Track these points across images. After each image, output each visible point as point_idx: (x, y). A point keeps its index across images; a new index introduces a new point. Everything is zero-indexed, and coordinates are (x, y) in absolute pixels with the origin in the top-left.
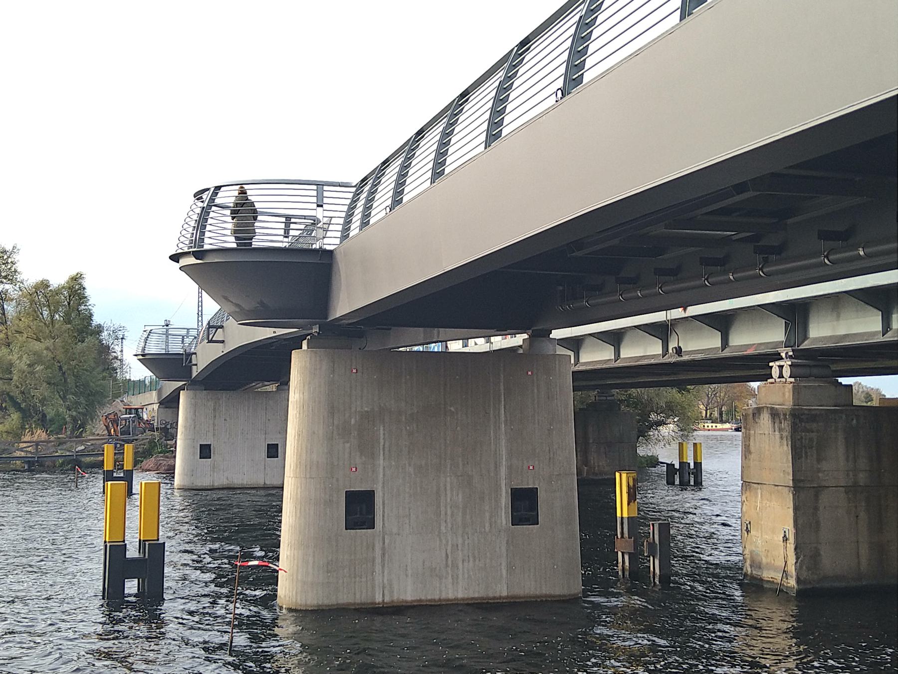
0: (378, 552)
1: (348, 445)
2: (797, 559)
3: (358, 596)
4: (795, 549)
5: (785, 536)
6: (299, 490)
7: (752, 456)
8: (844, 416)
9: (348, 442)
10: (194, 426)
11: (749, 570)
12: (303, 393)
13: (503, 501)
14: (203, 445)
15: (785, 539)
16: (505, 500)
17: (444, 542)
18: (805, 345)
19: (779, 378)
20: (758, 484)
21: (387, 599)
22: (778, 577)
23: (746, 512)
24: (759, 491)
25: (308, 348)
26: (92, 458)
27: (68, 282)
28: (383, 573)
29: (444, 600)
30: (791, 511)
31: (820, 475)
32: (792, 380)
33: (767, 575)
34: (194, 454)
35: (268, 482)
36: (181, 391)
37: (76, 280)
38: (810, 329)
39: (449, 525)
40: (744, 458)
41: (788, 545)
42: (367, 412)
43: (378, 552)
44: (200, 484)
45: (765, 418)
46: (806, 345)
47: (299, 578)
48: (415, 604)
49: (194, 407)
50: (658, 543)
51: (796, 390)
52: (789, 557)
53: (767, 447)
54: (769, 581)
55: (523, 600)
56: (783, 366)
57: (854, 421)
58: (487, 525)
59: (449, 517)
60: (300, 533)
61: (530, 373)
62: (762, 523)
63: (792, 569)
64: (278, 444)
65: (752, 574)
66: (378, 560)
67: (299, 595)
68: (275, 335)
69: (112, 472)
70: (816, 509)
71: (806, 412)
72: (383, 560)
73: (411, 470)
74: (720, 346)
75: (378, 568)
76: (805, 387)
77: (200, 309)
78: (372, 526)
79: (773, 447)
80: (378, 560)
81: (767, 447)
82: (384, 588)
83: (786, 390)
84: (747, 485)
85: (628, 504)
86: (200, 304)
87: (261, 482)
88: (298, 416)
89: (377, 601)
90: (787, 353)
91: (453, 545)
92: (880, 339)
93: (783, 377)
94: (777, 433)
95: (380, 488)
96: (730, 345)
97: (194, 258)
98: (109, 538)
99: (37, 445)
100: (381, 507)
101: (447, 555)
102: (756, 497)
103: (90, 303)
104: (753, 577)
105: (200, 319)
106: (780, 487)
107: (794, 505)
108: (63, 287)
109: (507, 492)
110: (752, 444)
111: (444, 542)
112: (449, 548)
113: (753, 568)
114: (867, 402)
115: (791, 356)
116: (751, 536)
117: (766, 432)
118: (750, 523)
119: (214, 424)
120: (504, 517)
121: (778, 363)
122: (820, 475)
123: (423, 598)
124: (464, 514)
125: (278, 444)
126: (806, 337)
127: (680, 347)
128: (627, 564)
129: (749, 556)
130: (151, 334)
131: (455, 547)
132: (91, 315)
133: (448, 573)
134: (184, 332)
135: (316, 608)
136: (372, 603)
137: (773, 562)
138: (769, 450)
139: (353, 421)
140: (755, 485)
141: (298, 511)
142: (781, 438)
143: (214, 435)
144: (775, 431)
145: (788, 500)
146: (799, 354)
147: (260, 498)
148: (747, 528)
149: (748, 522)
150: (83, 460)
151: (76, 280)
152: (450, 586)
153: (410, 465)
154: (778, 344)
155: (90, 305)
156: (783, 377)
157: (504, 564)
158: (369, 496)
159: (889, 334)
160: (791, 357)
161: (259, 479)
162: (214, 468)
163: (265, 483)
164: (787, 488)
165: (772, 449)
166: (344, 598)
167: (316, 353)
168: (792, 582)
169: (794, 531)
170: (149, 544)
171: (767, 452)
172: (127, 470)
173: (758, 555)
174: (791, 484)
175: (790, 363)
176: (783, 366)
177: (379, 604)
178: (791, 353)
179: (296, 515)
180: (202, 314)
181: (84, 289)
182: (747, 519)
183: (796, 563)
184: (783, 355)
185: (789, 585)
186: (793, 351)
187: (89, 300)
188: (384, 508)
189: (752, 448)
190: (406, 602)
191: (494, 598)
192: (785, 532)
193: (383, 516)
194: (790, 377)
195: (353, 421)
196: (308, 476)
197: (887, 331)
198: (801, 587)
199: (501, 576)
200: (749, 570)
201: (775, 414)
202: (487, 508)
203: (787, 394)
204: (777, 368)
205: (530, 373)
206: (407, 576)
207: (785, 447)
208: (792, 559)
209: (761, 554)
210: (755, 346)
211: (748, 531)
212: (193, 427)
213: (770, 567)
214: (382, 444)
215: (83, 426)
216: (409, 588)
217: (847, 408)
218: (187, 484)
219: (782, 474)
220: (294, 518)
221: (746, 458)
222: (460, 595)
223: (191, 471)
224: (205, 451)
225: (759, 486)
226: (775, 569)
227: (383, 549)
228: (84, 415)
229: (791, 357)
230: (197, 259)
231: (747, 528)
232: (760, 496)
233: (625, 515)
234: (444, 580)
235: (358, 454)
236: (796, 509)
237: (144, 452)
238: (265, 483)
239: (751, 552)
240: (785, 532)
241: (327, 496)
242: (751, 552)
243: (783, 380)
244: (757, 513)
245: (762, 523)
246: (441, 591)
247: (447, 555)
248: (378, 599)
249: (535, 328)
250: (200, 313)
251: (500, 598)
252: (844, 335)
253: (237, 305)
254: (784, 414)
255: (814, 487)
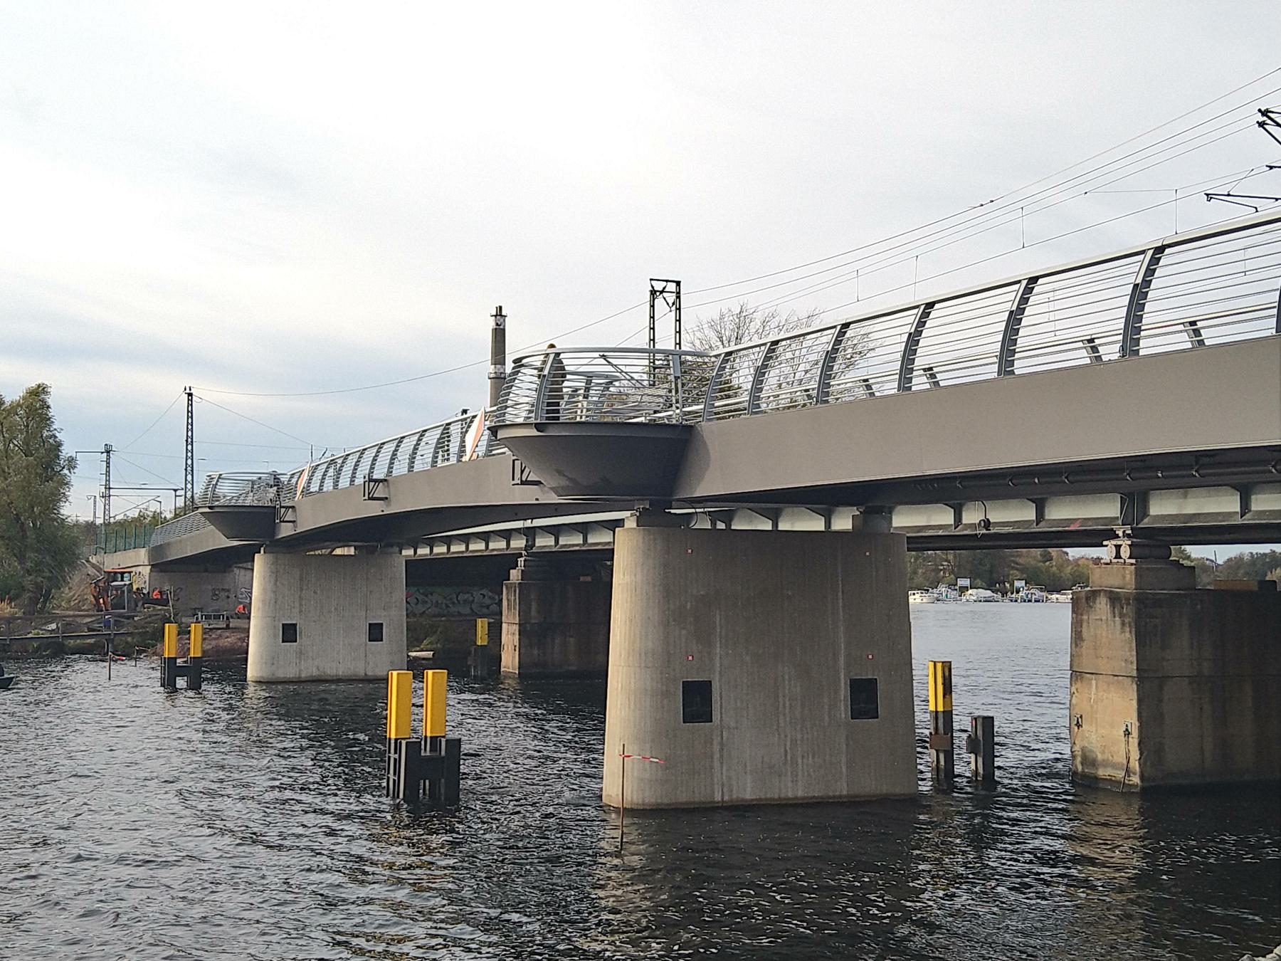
0: (716, 748)
1: (684, 632)
2: (1141, 754)
3: (697, 795)
4: (1139, 744)
5: (1127, 730)
6: (633, 680)
7: (1085, 644)
8: (1188, 602)
9: (684, 628)
10: (275, 600)
11: (1080, 768)
12: (635, 575)
13: (842, 693)
14: (286, 624)
15: (1127, 733)
16: (844, 691)
17: (783, 736)
18: (1145, 523)
19: (1115, 558)
20: (1092, 674)
21: (726, 798)
22: (1120, 775)
23: (1076, 705)
24: (1094, 682)
25: (638, 526)
26: (78, 641)
27: (24, 398)
28: (722, 769)
29: (785, 799)
30: (1135, 703)
31: (1165, 663)
32: (1133, 561)
33: (1102, 773)
34: (275, 636)
35: (369, 673)
36: (256, 555)
37: (38, 394)
38: (1151, 507)
39: (788, 719)
40: (1074, 645)
41: (1130, 739)
42: (703, 595)
43: (716, 748)
44: (282, 676)
45: (1102, 604)
46: (1147, 524)
47: (635, 774)
48: (755, 803)
49: (275, 575)
50: (981, 739)
51: (1139, 573)
52: (179, 869)
53: (1104, 634)
54: (1106, 779)
55: (863, 799)
56: (1120, 546)
57: (1199, 607)
58: (827, 718)
59: (787, 711)
60: (635, 727)
61: (868, 554)
62: (1098, 716)
63: (1135, 765)
64: (382, 624)
65: (1083, 771)
66: (717, 756)
67: (635, 793)
68: (537, 502)
69: (176, 658)
70: (1161, 701)
71: (1150, 596)
72: (722, 756)
73: (748, 658)
74: (1034, 518)
75: (717, 764)
76: (1147, 569)
77: (190, 434)
78: (710, 719)
79: (1112, 634)
80: (717, 756)
81: (1104, 634)
82: (723, 785)
83: (1127, 572)
84: (1077, 675)
85: (944, 697)
86: (190, 427)
87: (361, 672)
88: (629, 600)
89: (716, 799)
90: (1124, 532)
91: (791, 741)
92: (1239, 521)
93: (1121, 558)
94: (1117, 619)
95: (717, 679)
96: (1047, 518)
97: (535, 430)
98: (431, 732)
99: (228, 627)
100: (719, 698)
101: (786, 751)
102: (1091, 684)
103: (54, 427)
104: (1084, 776)
105: (190, 447)
106: (1120, 678)
107: (1138, 695)
108: (19, 405)
109: (845, 684)
110: (1084, 630)
111: (783, 736)
112: (788, 744)
113: (1085, 766)
114: (1044, 562)
115: (1129, 534)
116: (1083, 731)
117: (1104, 618)
118: (1081, 717)
119: (300, 597)
120: (843, 710)
121: (1114, 542)
122: (1165, 663)
123: (763, 797)
124: (803, 706)
125: (382, 624)
126: (1145, 514)
127: (988, 520)
128: (942, 762)
129: (1080, 753)
130: (220, 480)
131: (794, 742)
132: (60, 444)
133: (786, 770)
134: (255, 477)
135: (654, 807)
136: (711, 802)
137: (1111, 758)
138: (1107, 637)
139: (689, 606)
140: (1088, 675)
141: (632, 703)
142: (1123, 624)
143: (301, 611)
144: (1114, 617)
145: (1131, 692)
146: (1136, 533)
147: (357, 690)
148: (1078, 722)
149: (1078, 716)
150: (66, 643)
151: (38, 394)
152: (790, 784)
153: (747, 654)
154: (1113, 520)
155: (55, 430)
156: (1121, 558)
157: (844, 760)
158: (707, 685)
159: (1247, 516)
160: (1128, 536)
161: (359, 669)
162: (300, 654)
163: (366, 674)
164: (1130, 679)
165: (1110, 636)
166: (683, 797)
167: (649, 531)
168: (1136, 780)
169: (1137, 724)
170: (407, 743)
171: (1104, 640)
172: (194, 658)
173: (1091, 751)
174: (1135, 673)
175: (1129, 543)
176: (1120, 546)
177: (718, 802)
178: (1130, 532)
179: (629, 707)
180: (192, 442)
181: (48, 407)
182: (1077, 712)
183: (1140, 759)
184: (1120, 534)
185: (1131, 783)
186: (1132, 529)
187: (53, 422)
188: (721, 699)
189: (1085, 635)
190: (746, 800)
191: (834, 797)
192: (1127, 726)
193: (721, 708)
194: (1129, 558)
195: (689, 606)
196: (643, 665)
197: (1245, 513)
198: (1146, 784)
199: (841, 772)
200: (1080, 768)
201: (1114, 598)
202: (826, 700)
203: (1128, 577)
204: (1113, 547)
205: (868, 554)
206: (746, 773)
207: (1128, 635)
208: (1135, 754)
209: (1095, 750)
210: (1079, 521)
211: (1078, 725)
212: (273, 601)
213: (1106, 764)
214: (718, 631)
215: (47, 596)
216: (749, 790)
217: (1190, 592)
218: (266, 674)
219: (1124, 664)
220: (627, 709)
221: (1076, 645)
222: (800, 794)
223: (271, 658)
224: (289, 633)
225: (1093, 676)
226: (1115, 766)
227: (721, 744)
228: (49, 579)
229: (1128, 536)
230: (538, 431)
231: (1078, 722)
232: (1094, 687)
233: (940, 709)
234: (783, 777)
235: (694, 641)
236: (1140, 701)
237: (154, 633)
238: (366, 674)
239: (1083, 749)
240: (1127, 726)
241: (665, 688)
242: (1083, 749)
243: (1122, 561)
244: (1092, 706)
245: (1098, 716)
246: (780, 790)
247: (786, 751)
248: (718, 797)
249: (870, 504)
250: (190, 440)
251: (840, 797)
252: (1194, 514)
253: (570, 479)
254: (1126, 599)
255: (1158, 678)
